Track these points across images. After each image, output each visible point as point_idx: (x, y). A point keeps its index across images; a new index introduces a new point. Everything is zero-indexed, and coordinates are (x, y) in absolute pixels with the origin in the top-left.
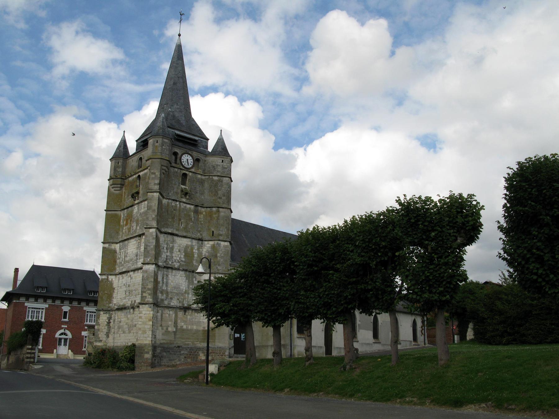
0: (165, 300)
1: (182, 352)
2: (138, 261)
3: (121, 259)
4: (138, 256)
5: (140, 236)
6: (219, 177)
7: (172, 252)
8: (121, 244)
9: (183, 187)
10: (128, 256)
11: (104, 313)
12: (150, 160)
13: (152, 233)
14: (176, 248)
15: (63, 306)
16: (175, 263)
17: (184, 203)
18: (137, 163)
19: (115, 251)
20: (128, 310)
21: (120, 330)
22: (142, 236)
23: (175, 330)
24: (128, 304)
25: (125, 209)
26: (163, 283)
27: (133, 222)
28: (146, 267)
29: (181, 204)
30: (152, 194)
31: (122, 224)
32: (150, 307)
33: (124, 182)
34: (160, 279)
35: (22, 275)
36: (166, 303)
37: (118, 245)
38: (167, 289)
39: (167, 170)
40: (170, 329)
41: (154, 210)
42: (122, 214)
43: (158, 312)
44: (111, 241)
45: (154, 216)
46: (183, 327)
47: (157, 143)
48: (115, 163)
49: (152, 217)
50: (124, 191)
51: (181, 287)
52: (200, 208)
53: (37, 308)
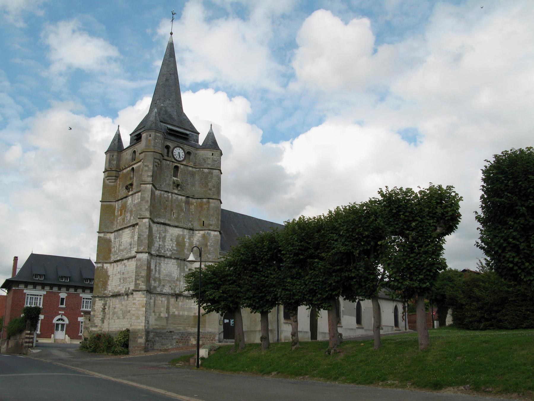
0: (158, 287)
1: (174, 337)
2: (132, 249)
3: (116, 248)
4: (132, 245)
5: (134, 226)
6: (209, 170)
7: (164, 241)
8: (116, 233)
9: (175, 179)
10: (122, 245)
11: (99, 300)
12: (144, 153)
13: (145, 223)
14: (168, 237)
15: (61, 292)
16: (167, 252)
17: (176, 194)
18: (131, 156)
19: (110, 241)
20: (123, 297)
21: (115, 316)
22: (135, 226)
23: (167, 316)
24: (123, 291)
25: (119, 200)
26: (156, 271)
27: (127, 212)
28: (139, 256)
29: (173, 195)
30: (145, 185)
31: (116, 214)
32: (144, 294)
33: (119, 174)
34: (153, 267)
35: (21, 264)
36: (159, 290)
37: (113, 234)
38: (159, 276)
39: (159, 162)
40: (162, 315)
41: (147, 201)
42: (116, 205)
43: (151, 299)
44: (106, 230)
45: (147, 207)
46: (174, 313)
47: (150, 137)
48: (110, 155)
49: (145, 207)
50: (118, 183)
51: (173, 275)
52: (191, 199)
53: (35, 295)
